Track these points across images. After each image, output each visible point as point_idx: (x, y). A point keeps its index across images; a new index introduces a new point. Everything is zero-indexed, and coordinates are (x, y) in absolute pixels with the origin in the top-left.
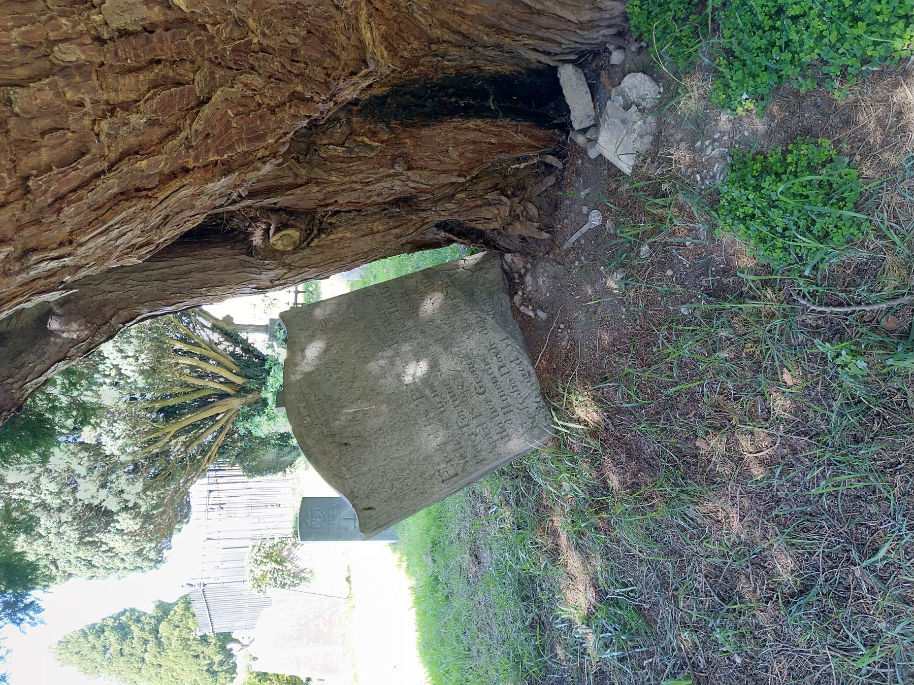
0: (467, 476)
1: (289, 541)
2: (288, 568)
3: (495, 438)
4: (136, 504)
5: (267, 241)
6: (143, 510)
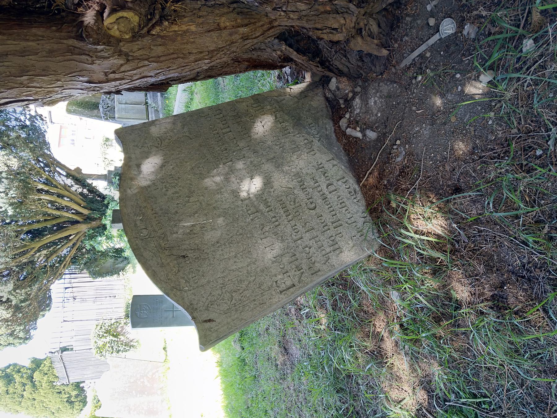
0: (304, 286)
1: (122, 321)
2: (121, 339)
3: (328, 250)
4: (8, 299)
5: (100, 22)
6: (14, 303)
